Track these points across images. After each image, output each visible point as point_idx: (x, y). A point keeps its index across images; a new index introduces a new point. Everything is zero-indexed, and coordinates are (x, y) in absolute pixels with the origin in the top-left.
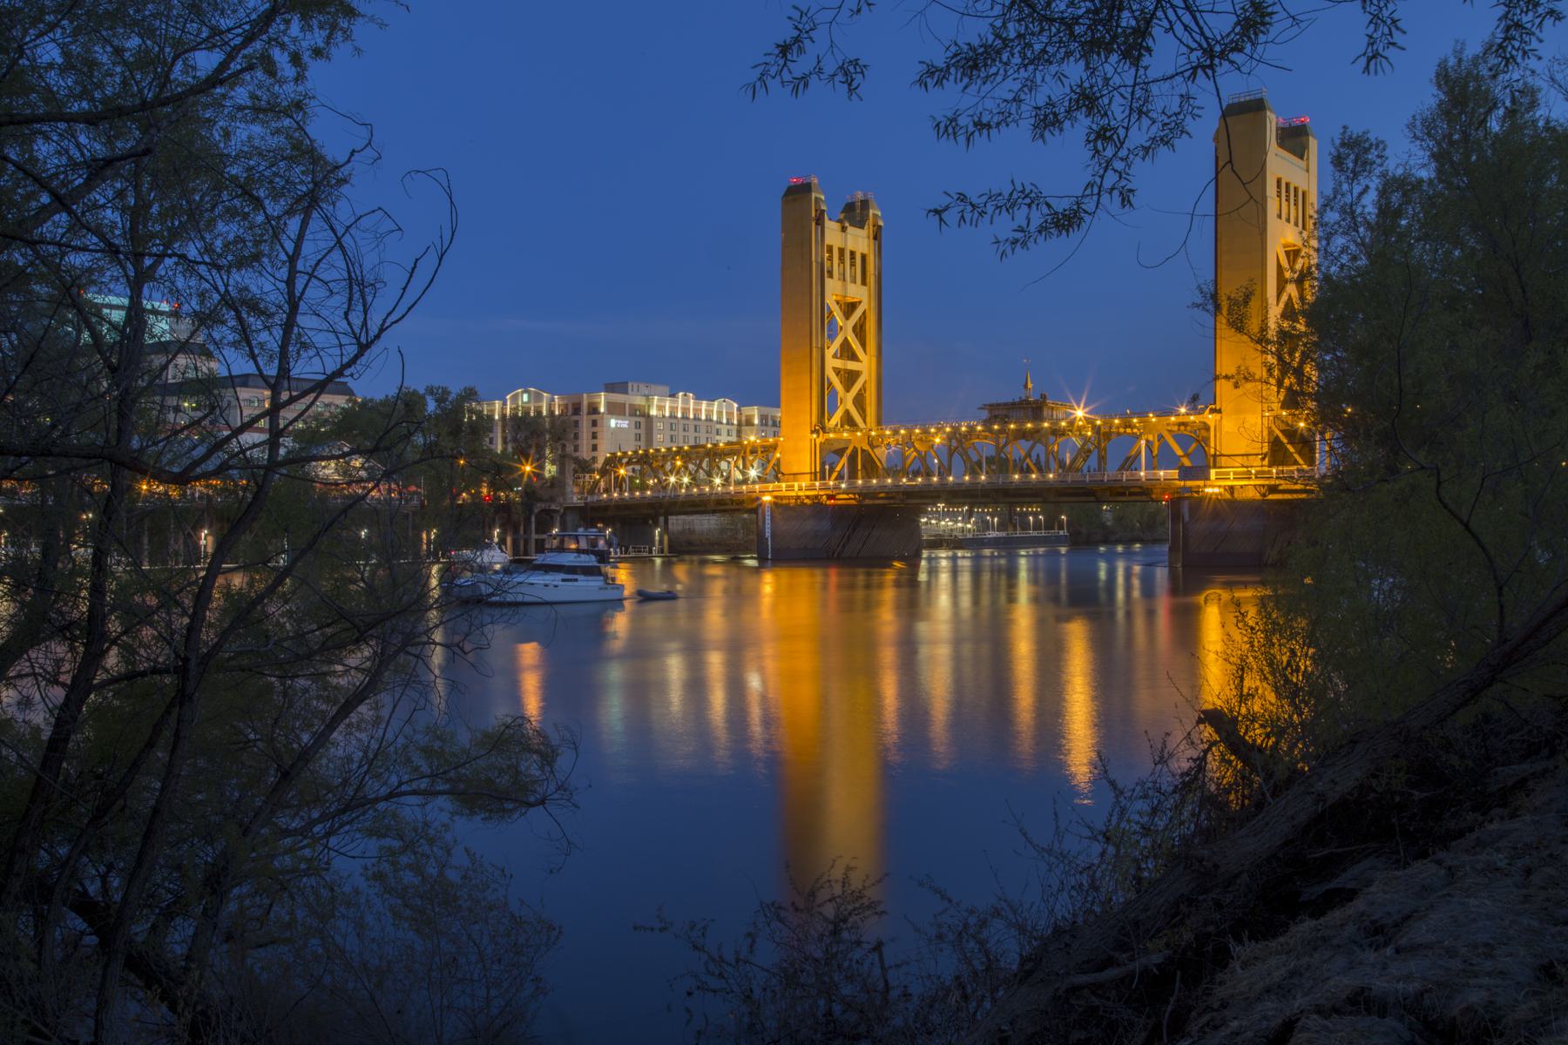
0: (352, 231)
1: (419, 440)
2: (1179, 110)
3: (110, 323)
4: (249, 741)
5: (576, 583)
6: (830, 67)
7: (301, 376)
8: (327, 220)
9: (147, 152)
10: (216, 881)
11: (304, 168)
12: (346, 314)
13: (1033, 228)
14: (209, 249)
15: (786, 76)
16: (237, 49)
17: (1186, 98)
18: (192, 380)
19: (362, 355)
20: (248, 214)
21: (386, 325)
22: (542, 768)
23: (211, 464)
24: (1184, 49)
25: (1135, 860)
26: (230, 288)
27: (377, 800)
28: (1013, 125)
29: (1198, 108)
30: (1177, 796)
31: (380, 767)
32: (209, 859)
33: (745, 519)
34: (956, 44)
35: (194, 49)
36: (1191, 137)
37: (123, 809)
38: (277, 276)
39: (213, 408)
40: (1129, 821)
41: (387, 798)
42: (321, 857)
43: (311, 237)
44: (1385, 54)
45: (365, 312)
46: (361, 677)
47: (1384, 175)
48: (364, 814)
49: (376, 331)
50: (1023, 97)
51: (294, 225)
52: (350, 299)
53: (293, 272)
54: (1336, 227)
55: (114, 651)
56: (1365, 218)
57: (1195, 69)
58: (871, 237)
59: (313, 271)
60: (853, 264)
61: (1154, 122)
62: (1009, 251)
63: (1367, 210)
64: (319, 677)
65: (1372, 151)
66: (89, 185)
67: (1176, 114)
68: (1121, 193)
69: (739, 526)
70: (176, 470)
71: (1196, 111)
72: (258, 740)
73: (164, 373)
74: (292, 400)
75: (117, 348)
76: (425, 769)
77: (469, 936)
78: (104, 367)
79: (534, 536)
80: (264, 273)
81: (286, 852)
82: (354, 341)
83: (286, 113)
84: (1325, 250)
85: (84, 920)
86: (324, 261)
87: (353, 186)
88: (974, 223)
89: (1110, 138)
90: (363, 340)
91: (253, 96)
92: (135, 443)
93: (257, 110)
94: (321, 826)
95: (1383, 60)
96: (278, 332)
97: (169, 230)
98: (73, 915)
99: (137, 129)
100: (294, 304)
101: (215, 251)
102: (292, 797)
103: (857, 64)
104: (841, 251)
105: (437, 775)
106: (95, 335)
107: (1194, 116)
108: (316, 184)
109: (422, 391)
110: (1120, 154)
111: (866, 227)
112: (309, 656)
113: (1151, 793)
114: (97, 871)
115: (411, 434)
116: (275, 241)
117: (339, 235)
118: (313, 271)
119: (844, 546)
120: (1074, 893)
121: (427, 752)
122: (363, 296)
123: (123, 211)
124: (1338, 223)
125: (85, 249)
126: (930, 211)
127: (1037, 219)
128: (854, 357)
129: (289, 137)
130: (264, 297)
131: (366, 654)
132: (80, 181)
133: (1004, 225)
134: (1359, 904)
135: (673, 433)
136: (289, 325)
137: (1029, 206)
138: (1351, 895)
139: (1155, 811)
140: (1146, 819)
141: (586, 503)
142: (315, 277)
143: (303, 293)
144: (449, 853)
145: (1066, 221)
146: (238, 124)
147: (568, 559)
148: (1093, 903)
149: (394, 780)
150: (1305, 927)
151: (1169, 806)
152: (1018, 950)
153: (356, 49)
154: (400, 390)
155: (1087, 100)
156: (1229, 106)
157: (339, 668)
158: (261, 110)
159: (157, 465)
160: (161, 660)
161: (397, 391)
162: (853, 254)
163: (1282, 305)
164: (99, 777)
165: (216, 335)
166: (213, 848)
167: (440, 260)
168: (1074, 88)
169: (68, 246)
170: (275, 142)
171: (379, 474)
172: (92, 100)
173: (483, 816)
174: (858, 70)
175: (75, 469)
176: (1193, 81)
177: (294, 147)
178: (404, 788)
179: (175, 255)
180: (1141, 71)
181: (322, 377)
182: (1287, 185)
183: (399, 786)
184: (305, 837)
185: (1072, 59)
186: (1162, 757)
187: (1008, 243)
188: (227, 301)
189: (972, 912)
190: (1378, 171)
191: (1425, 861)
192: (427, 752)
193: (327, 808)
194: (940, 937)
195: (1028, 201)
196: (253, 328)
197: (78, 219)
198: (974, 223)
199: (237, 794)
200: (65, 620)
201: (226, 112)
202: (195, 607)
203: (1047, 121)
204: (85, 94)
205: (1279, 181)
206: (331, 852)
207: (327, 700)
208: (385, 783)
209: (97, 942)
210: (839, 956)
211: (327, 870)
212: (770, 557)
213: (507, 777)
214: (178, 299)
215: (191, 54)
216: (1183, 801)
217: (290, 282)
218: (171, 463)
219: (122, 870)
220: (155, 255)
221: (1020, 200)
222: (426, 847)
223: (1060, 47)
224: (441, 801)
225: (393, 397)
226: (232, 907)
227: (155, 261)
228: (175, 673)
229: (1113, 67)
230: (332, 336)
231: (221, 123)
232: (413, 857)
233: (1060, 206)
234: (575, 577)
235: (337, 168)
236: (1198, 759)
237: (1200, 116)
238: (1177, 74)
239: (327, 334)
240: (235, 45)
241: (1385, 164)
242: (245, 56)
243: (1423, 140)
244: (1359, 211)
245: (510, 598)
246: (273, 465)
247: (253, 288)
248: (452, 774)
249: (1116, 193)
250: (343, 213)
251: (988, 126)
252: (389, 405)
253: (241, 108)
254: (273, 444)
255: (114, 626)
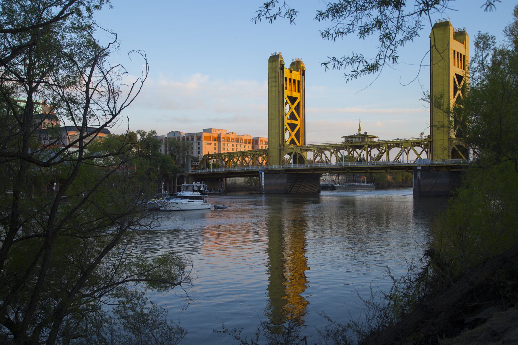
0: (110, 73)
1: (134, 150)
2: (415, 26)
3: (19, 107)
4: (72, 261)
5: (193, 203)
6: (284, 12)
7: (91, 127)
8: (100, 69)
9: (34, 44)
10: (59, 314)
11: (92, 50)
12: (108, 104)
13: (359, 70)
14: (56, 80)
15: (268, 15)
16: (67, 6)
17: (418, 22)
18: (50, 128)
19: (114, 119)
20: (71, 67)
21: (122, 107)
22: (179, 271)
23: (57, 159)
24: (417, 4)
25: (401, 306)
26: (65, 94)
27: (118, 283)
28: (352, 33)
29: (423, 26)
30: (417, 282)
31: (120, 271)
32: (56, 306)
33: (255, 179)
34: (331, 4)
35: (51, 6)
36: (419, 36)
37: (24, 287)
38: (82, 89)
39: (58, 139)
40: (399, 292)
41: (122, 282)
42: (97, 305)
43: (95, 75)
44: (494, 4)
45: (115, 103)
46: (112, 237)
47: (495, 49)
48: (113, 288)
49: (119, 110)
50: (355, 23)
51: (88, 71)
52: (109, 98)
53: (88, 88)
54: (476, 69)
55: (21, 228)
56: (487, 65)
57: (421, 11)
58: (301, 75)
59: (95, 88)
60: (295, 85)
61: (404, 32)
62: (350, 79)
63: (488, 62)
64: (96, 237)
65: (490, 40)
66: (12, 57)
67: (414, 28)
68: (393, 58)
69: (253, 181)
70: (45, 161)
71: (421, 27)
72: (75, 261)
73: (40, 125)
74: (88, 135)
75: (23, 116)
76: (136, 272)
77: (152, 334)
78: (18, 123)
79: (177, 185)
80: (77, 89)
81: (84, 303)
82: (111, 113)
83: (85, 29)
84: (472, 77)
85: (9, 329)
86: (99, 84)
87: (109, 56)
88: (338, 68)
89: (389, 37)
90: (114, 113)
91: (73, 23)
92: (29, 152)
93: (74, 28)
94: (98, 293)
95: (492, 6)
96: (82, 111)
97: (42, 73)
98: (4, 327)
99: (30, 35)
100: (88, 100)
101: (59, 81)
102: (87, 282)
103: (294, 11)
104: (290, 80)
105: (140, 274)
106: (15, 112)
107: (421, 29)
108: (97, 56)
109: (135, 132)
110: (393, 43)
111: (299, 71)
112: (93, 230)
113: (407, 281)
114: (14, 310)
115: (132, 148)
116: (81, 77)
117: (105, 74)
118: (95, 88)
119: (291, 189)
120: (378, 319)
121: (137, 265)
122: (114, 97)
123: (25, 65)
124: (477, 67)
125: (10, 80)
126: (322, 64)
127: (361, 67)
128: (295, 119)
129: (86, 38)
130: (77, 97)
131: (114, 229)
132: (9, 55)
133: (349, 69)
134: (487, 324)
135: (228, 147)
136: (87, 108)
137: (359, 62)
138: (484, 321)
139: (409, 288)
140: (405, 291)
141: (196, 173)
142: (96, 90)
143: (91, 96)
144: (145, 303)
145: (372, 68)
146: (67, 33)
147: (190, 194)
148: (385, 323)
149: (125, 275)
150: (467, 333)
151: (414, 286)
152: (357, 340)
153: (111, 6)
154: (128, 132)
155: (379, 24)
156: (435, 25)
157: (104, 234)
158: (75, 28)
159: (38, 159)
160: (38, 231)
161: (126, 132)
162: (294, 81)
163: (455, 99)
164: (15, 275)
165: (60, 112)
166: (57, 301)
167: (142, 83)
168: (375, 19)
169: (5, 79)
170: (80, 40)
171: (119, 162)
172: (13, 25)
173: (158, 289)
174: (294, 13)
175: (7, 161)
176: (421, 16)
177: (88, 42)
178: (129, 279)
179: (44, 82)
180: (401, 12)
181: (99, 127)
182: (461, 54)
183: (127, 278)
184: (92, 297)
185: (374, 8)
186: (411, 268)
187: (350, 76)
188: (63, 99)
189: (340, 326)
190: (492, 48)
191: (513, 308)
192: (137, 265)
193: (100, 286)
194: (328, 335)
195: (359, 60)
196: (74, 109)
197: (9, 69)
198: (338, 68)
199: (66, 281)
200: (3, 217)
201: (62, 29)
202: (51, 212)
203: (365, 31)
204: (11, 22)
205: (454, 51)
206: (101, 303)
207: (100, 246)
208: (121, 277)
209: (13, 337)
210: (291, 342)
211: (100, 309)
212: (264, 193)
213: (166, 275)
214: (45, 98)
215: (50, 8)
216: (419, 284)
217: (87, 92)
218: (43, 158)
219: (23, 310)
220: (37, 82)
221: (356, 60)
222: (136, 301)
223: (369, 4)
224: (142, 283)
225: (125, 134)
226: (64, 323)
227: (37, 84)
228: (44, 236)
229: (390, 11)
230: (102, 112)
231: (60, 33)
232: (131, 305)
233: (371, 62)
234: (193, 200)
235: (104, 50)
236: (425, 268)
237: (423, 29)
238: (415, 13)
239: (100, 111)
240: (66, 5)
241: (495, 45)
242: (69, 9)
243: (510, 36)
244: (485, 63)
245: (168, 208)
246: (80, 159)
247: (73, 94)
248: (146, 273)
249: (391, 58)
250: (106, 66)
251: (343, 33)
252: (122, 138)
253: (68, 28)
254: (80, 151)
255: (21, 219)
